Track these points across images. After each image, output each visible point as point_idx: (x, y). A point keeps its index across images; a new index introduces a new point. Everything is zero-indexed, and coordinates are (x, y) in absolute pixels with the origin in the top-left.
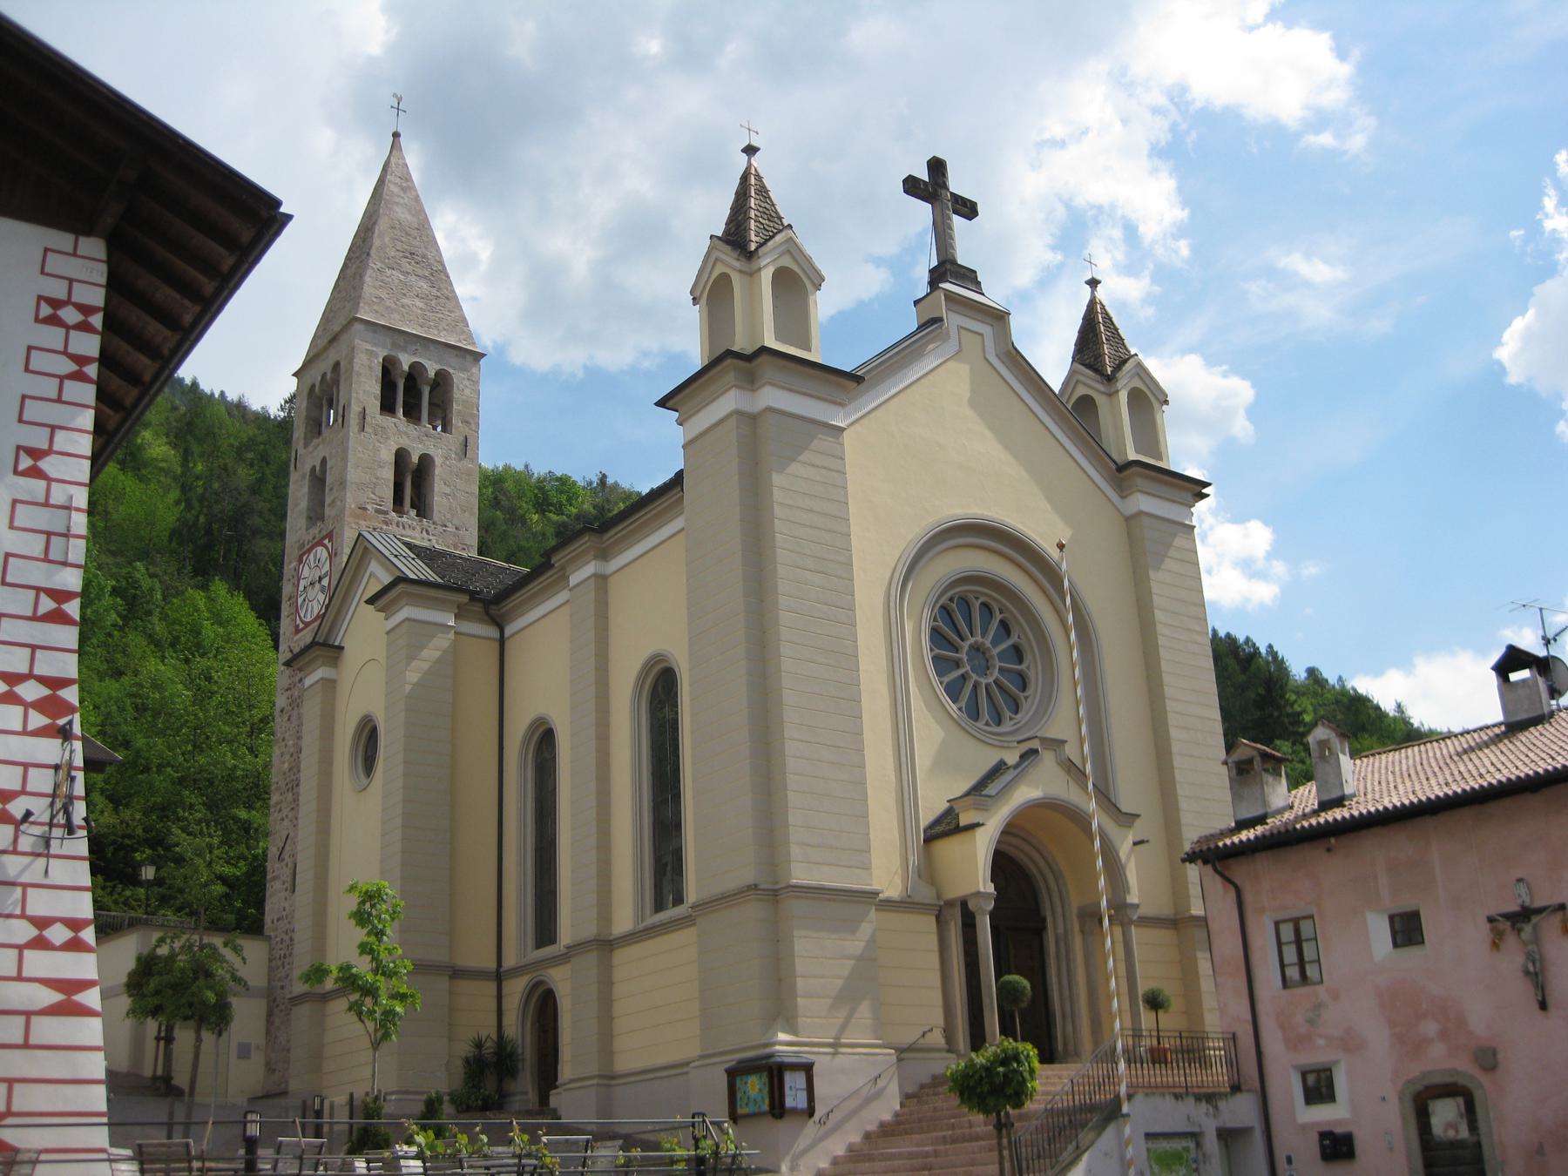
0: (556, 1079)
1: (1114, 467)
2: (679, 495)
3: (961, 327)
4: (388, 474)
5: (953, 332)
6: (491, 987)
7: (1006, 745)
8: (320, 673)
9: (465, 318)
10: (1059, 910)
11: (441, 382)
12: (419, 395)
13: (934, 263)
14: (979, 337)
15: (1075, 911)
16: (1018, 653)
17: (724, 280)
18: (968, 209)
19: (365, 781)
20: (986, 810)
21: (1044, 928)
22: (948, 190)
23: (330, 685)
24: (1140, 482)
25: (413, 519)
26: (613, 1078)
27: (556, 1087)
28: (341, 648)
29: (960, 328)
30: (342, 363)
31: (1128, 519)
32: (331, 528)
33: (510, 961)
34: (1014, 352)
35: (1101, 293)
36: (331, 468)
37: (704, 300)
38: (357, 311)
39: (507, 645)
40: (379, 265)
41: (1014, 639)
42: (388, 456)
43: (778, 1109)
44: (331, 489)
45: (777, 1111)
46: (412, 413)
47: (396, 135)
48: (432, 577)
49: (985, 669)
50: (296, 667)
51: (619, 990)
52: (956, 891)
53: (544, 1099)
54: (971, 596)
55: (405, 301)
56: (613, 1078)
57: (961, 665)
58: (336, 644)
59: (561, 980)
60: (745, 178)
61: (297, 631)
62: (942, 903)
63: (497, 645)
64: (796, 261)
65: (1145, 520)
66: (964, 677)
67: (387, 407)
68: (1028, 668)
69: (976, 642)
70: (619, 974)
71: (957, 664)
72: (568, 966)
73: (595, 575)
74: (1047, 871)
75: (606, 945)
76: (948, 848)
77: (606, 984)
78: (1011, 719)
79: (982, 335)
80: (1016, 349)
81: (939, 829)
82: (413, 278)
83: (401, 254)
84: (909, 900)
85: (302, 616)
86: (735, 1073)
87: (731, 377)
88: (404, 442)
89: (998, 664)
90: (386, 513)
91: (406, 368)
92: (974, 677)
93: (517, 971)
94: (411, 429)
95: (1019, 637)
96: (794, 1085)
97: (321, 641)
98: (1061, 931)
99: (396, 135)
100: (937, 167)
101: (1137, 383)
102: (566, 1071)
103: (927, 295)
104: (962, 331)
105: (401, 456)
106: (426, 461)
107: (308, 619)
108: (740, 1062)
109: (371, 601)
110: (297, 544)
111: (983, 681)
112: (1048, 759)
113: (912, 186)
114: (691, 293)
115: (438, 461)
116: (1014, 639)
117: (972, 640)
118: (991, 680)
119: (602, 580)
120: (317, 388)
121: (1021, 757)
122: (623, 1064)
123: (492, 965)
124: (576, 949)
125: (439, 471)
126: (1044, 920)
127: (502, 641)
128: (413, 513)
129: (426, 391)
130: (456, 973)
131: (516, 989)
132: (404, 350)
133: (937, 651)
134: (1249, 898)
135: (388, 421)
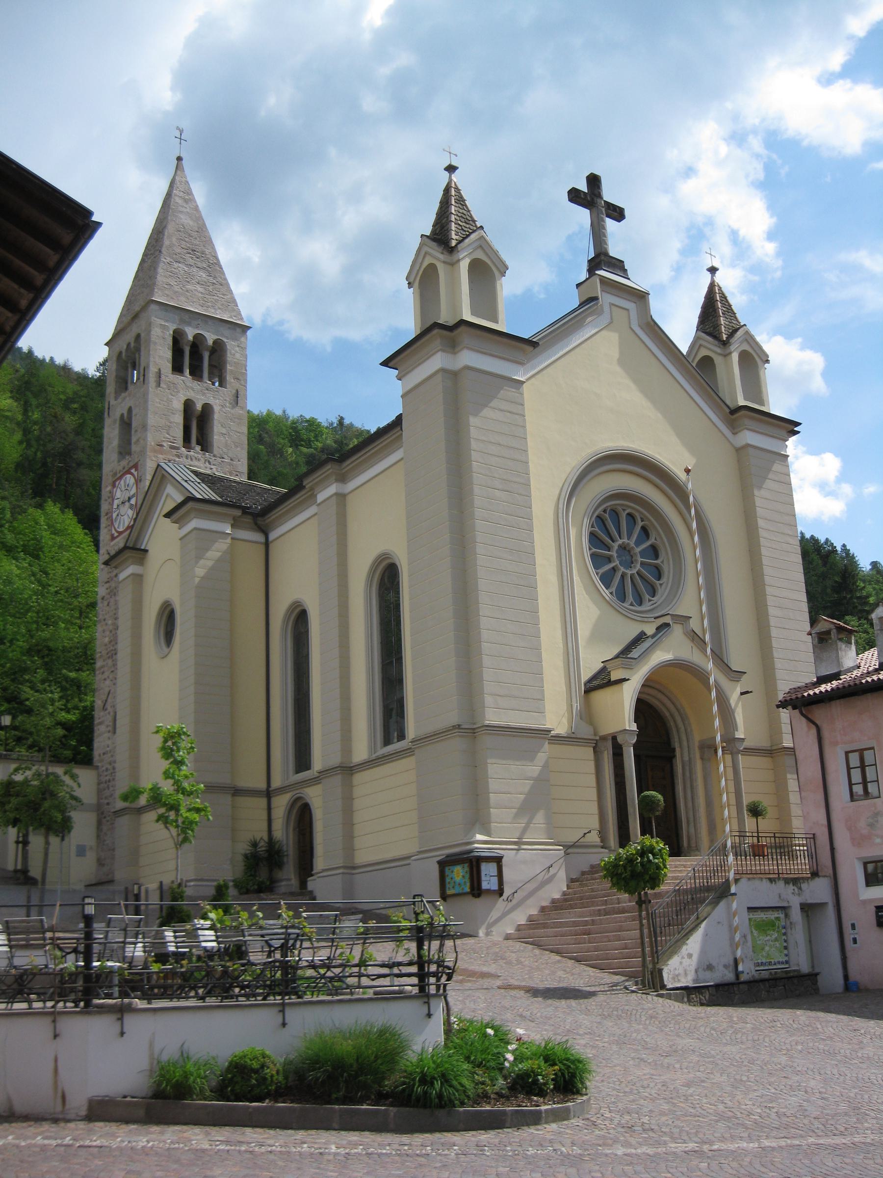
0: (312, 869)
1: (728, 411)
2: (398, 434)
3: (613, 305)
4: (179, 419)
5: (606, 308)
6: (263, 802)
7: (646, 620)
8: (131, 569)
9: (235, 300)
10: (685, 743)
11: (218, 349)
12: (200, 359)
13: (592, 255)
14: (625, 312)
15: (697, 744)
16: (654, 551)
17: (432, 268)
18: (618, 214)
19: (166, 650)
20: (632, 669)
21: (674, 756)
22: (602, 198)
23: (138, 578)
24: (747, 422)
25: (198, 453)
26: (354, 868)
27: (312, 875)
28: (146, 551)
29: (612, 305)
30: (143, 335)
31: (738, 450)
32: (136, 460)
33: (276, 783)
34: (652, 323)
35: (719, 278)
36: (136, 415)
37: (416, 284)
38: (152, 295)
39: (271, 546)
40: (169, 260)
41: (651, 541)
42: (178, 405)
43: (476, 891)
44: (136, 431)
45: (476, 892)
46: (196, 372)
47: (179, 159)
48: (214, 496)
49: (630, 564)
50: (114, 565)
51: (357, 804)
52: (608, 728)
53: (303, 884)
54: (620, 509)
55: (189, 287)
56: (354, 868)
57: (612, 559)
58: (143, 548)
59: (315, 796)
60: (447, 190)
61: (113, 538)
62: (598, 738)
63: (262, 548)
64: (487, 255)
65: (751, 451)
66: (614, 569)
67: (177, 368)
68: (662, 562)
69: (623, 543)
70: (357, 791)
71: (609, 559)
72: (320, 786)
73: (336, 494)
74: (676, 714)
75: (348, 770)
76: (602, 697)
77: (348, 800)
78: (650, 600)
79: (627, 310)
80: (653, 321)
81: (595, 683)
82: (195, 270)
83: (185, 251)
84: (573, 736)
85: (116, 526)
86: (444, 864)
87: (437, 343)
88: (191, 395)
89: (640, 560)
90: (178, 448)
91: (191, 338)
92: (622, 569)
93: (282, 790)
94: (196, 385)
95: (656, 539)
96: (488, 871)
97: (131, 546)
98: (686, 758)
99: (179, 159)
100: (594, 181)
101: (746, 347)
102: (320, 863)
103: (587, 279)
104: (613, 307)
105: (188, 405)
106: (207, 409)
107: (121, 529)
108: (448, 856)
109: (168, 515)
110: (111, 473)
111: (629, 572)
112: (677, 631)
113: (575, 196)
114: (407, 279)
115: (216, 408)
116: (651, 541)
117: (620, 542)
118: (634, 571)
119: (341, 497)
120: (124, 354)
121: (657, 629)
122: (362, 857)
123: (263, 786)
124: (325, 773)
125: (217, 416)
126: (674, 750)
127: (267, 544)
128: (198, 448)
129: (206, 356)
130: (237, 792)
131: (281, 803)
132: (189, 324)
133: (594, 550)
134: (826, 734)
135: (178, 379)
